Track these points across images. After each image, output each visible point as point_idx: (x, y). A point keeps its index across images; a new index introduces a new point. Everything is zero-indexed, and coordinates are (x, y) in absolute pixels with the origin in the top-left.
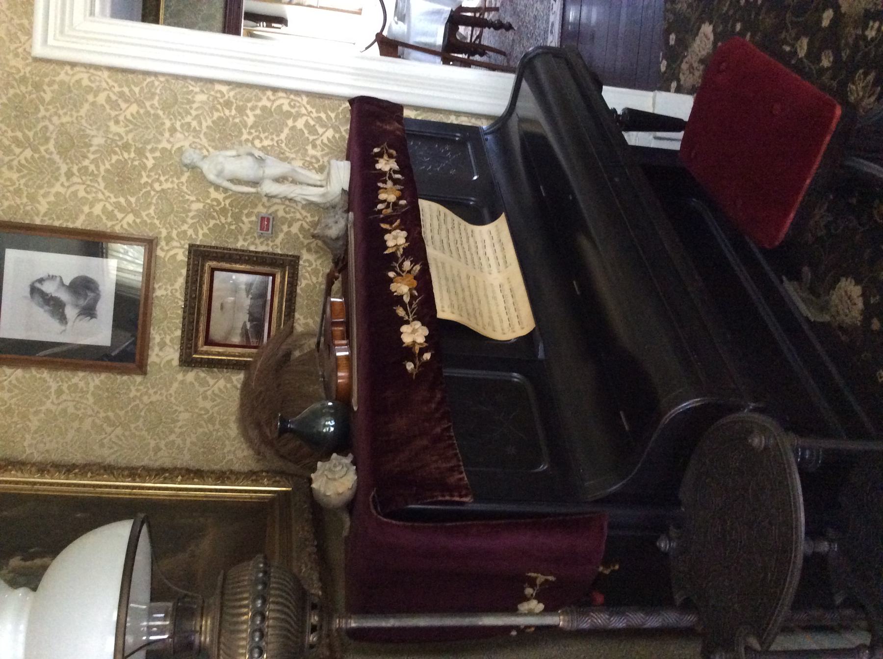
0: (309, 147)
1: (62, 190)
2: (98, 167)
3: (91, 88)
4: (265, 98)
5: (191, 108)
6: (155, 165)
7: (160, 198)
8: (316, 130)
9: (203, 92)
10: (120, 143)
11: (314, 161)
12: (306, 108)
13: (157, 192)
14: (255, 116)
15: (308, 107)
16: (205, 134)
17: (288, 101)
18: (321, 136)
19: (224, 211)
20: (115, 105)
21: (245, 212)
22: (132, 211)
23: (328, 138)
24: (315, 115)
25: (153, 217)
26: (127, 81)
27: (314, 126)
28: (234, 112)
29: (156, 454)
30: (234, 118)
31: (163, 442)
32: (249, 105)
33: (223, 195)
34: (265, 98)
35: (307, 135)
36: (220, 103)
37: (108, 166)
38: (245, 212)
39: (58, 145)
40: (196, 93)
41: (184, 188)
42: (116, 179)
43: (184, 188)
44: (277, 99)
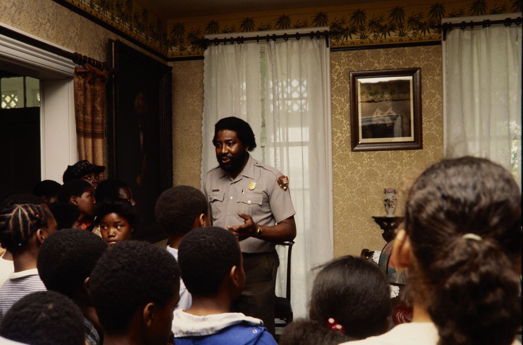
0: (351, 172)
1: (344, 123)
2: (374, 167)
3: (402, 163)
4: (346, 121)
5: (339, 97)
6: (378, 186)
7: (346, 155)
8: (337, 140)
9: (386, 167)
10: (384, 173)
11: (346, 173)
12: (365, 169)
13: (368, 187)
14: (339, 118)
15: (345, 137)
16: (371, 169)
17: (367, 163)
18: (356, 176)
19: (344, 177)
20: (397, 172)
21: (345, 184)
22: (340, 146)
23: (335, 145)
24: (343, 139)
25: (338, 153)
26: (345, 75)
27: (339, 139)
28: (339, 111)
29: (191, 97)
30: (338, 111)
31: (195, 99)
32: (343, 116)
33: (350, 176)
34: (346, 121)
35: (335, 137)
36: (383, 173)
37: (375, 170)
38: (345, 184)
39: (339, 87)
40: (344, 98)
41: (350, 162)
42: (371, 173)
43: (350, 162)
44: (367, 159)
